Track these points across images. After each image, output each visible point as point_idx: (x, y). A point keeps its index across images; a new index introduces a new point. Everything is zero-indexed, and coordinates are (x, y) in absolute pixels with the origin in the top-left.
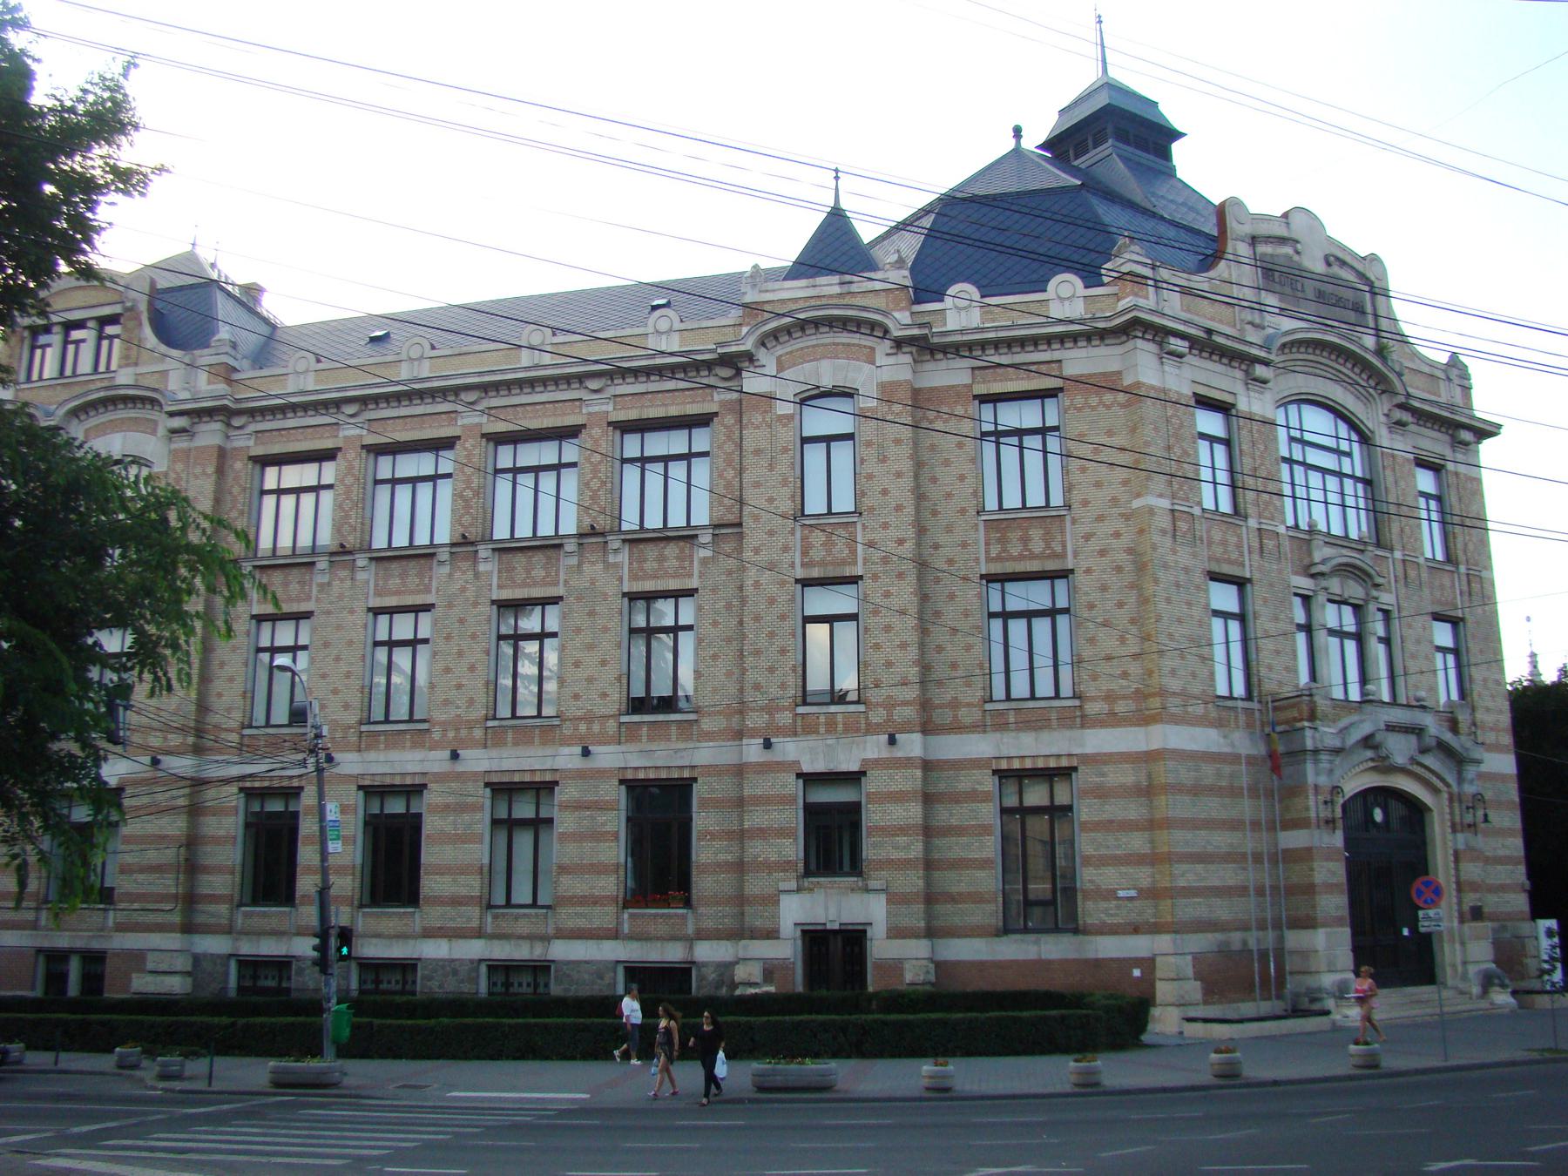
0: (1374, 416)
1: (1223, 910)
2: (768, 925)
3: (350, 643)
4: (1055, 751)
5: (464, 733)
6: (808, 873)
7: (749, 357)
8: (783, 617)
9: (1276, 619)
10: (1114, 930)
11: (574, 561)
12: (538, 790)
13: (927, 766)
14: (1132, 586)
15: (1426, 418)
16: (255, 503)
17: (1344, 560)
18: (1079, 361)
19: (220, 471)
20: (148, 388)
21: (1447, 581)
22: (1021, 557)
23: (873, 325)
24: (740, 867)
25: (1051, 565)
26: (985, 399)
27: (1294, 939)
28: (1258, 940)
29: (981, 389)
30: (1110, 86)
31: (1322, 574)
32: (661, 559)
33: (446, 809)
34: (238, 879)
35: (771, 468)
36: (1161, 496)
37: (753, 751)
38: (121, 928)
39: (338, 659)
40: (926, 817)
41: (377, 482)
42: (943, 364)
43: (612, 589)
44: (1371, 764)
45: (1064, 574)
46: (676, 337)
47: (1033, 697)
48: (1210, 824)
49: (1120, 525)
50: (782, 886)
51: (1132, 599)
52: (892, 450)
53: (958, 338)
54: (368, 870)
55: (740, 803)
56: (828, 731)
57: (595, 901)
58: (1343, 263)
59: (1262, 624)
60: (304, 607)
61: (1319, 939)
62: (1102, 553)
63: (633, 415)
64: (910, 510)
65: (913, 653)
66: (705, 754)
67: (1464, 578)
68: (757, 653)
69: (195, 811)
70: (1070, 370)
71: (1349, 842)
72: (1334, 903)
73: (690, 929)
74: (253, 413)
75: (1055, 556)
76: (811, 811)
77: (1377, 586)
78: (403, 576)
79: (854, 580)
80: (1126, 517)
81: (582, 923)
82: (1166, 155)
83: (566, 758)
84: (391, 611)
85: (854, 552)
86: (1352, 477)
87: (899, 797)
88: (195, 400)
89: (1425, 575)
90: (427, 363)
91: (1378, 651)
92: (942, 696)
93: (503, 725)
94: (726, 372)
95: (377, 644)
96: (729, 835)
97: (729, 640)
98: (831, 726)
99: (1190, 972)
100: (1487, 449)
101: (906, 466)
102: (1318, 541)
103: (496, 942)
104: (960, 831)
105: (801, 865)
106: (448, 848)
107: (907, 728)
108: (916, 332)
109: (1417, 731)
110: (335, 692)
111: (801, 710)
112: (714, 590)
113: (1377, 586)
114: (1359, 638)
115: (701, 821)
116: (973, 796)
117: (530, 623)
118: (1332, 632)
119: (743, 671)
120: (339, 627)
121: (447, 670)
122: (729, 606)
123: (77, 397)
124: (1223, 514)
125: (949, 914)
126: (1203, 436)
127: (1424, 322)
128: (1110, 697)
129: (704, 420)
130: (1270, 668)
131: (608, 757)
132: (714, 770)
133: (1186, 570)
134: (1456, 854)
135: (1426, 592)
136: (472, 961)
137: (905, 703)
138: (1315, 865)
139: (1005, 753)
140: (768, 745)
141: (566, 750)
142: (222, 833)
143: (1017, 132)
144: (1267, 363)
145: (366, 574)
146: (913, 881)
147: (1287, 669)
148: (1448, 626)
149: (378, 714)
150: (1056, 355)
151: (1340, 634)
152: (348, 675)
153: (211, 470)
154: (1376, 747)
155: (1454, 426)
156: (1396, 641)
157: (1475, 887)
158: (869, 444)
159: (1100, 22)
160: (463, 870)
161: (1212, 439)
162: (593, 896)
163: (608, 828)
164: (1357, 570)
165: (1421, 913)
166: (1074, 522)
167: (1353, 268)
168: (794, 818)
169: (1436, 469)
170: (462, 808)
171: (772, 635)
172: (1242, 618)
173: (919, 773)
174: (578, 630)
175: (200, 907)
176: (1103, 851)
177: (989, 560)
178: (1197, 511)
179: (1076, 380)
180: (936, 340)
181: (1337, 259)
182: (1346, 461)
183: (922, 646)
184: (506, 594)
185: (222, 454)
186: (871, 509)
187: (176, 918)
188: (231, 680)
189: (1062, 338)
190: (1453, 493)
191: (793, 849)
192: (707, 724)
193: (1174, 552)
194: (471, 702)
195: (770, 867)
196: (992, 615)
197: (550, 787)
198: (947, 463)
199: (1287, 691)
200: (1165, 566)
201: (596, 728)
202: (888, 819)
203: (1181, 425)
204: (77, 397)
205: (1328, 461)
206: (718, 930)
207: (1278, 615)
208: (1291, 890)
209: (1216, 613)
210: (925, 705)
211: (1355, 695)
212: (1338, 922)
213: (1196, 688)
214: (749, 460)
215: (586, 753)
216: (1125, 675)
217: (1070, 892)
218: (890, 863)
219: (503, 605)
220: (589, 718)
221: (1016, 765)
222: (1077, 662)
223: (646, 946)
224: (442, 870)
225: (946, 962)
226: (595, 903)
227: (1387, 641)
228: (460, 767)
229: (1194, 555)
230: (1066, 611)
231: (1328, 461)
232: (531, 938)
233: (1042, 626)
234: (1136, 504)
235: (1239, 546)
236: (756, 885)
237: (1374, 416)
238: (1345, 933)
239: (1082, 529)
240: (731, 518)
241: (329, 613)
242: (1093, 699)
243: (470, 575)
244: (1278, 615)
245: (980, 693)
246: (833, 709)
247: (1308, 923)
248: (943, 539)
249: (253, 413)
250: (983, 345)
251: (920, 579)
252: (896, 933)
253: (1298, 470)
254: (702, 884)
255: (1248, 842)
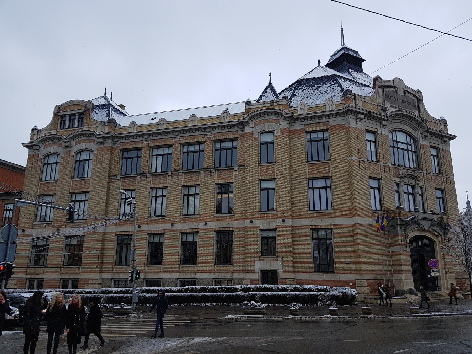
0: (418, 135)
1: (375, 268)
2: (252, 269)
3: (146, 197)
4: (327, 224)
5: (175, 219)
6: (262, 255)
7: (247, 123)
8: (255, 189)
9: (389, 189)
10: (344, 273)
11: (203, 175)
12: (186, 234)
13: (293, 227)
14: (347, 180)
15: (434, 134)
16: (121, 161)
17: (408, 173)
18: (333, 121)
19: (111, 153)
20: (91, 131)
21: (440, 179)
22: (317, 173)
23: (279, 114)
24: (245, 254)
25: (325, 175)
26: (308, 132)
27: (395, 277)
28: (385, 277)
29: (307, 130)
30: (344, 48)
31: (402, 177)
32: (225, 175)
33: (170, 239)
34: (115, 258)
35: (252, 151)
36: (356, 156)
37: (248, 223)
38: (83, 272)
39: (142, 201)
40: (293, 241)
41: (153, 156)
42: (297, 124)
43: (212, 183)
44: (417, 229)
45: (329, 177)
46: (228, 118)
47: (321, 210)
48: (370, 244)
49: (344, 164)
50: (256, 259)
51: (348, 184)
52: (284, 146)
53: (301, 116)
54: (149, 256)
55: (245, 237)
56: (267, 218)
57: (208, 263)
58: (409, 93)
59: (385, 190)
60: (133, 188)
61: (403, 276)
62: (339, 172)
63: (218, 138)
64: (288, 161)
65: (289, 198)
66: (236, 224)
67: (445, 178)
68: (249, 198)
69: (104, 241)
70: (331, 124)
71: (411, 250)
72: (407, 267)
73: (232, 270)
74: (120, 138)
75: (326, 173)
76: (262, 238)
77: (418, 180)
78: (129, 182)
79: (274, 179)
80: (346, 162)
81: (204, 268)
82: (360, 66)
83: (201, 225)
84: (156, 189)
85: (273, 172)
86: (411, 151)
87: (285, 235)
88: (104, 134)
89: (433, 177)
90: (165, 125)
91: (418, 198)
92: (296, 209)
93: (186, 216)
94: (241, 127)
95: (152, 197)
96: (242, 245)
97: (242, 195)
98: (268, 218)
99: (366, 285)
100: (452, 142)
101: (287, 150)
102: (401, 168)
103: (182, 274)
104: (302, 245)
105: (260, 253)
106: (170, 249)
107: (287, 217)
108: (290, 115)
109: (431, 220)
110: (142, 209)
111: (260, 213)
112: (238, 182)
113: (418, 180)
114: (413, 194)
115: (235, 241)
116: (305, 235)
117: (192, 191)
118: (405, 193)
119: (245, 203)
120: (143, 193)
121: (171, 203)
122: (242, 186)
123: (72, 134)
124: (373, 161)
125: (299, 267)
126: (368, 140)
127: (433, 108)
128: (342, 210)
129: (236, 139)
130: (387, 202)
131: (211, 225)
132: (238, 228)
133: (363, 176)
134: (444, 254)
135: (433, 182)
136: (175, 279)
137: (287, 211)
138: (402, 256)
139: (314, 224)
140: (252, 222)
141: (201, 223)
142: (111, 246)
143: (319, 61)
144: (386, 120)
145: (150, 179)
146: (290, 258)
147: (392, 203)
148: (440, 191)
149: (153, 215)
150: (327, 120)
151: (408, 193)
152: (145, 205)
153: (109, 152)
154: (419, 224)
155: (440, 136)
156: (424, 196)
157: (450, 264)
158: (278, 145)
159: (343, 30)
160: (174, 255)
161: (370, 141)
162: (207, 261)
163: (211, 243)
164: (412, 177)
165: (432, 270)
166: (332, 164)
167: (413, 95)
168: (258, 240)
169: (437, 148)
170: (174, 239)
171: (253, 194)
172: (379, 189)
173: (291, 229)
174: (204, 193)
175: (104, 266)
176: (341, 251)
177: (309, 174)
178: (366, 160)
179: (334, 126)
180: (295, 117)
181: (407, 91)
182: (409, 147)
183: (291, 196)
184: (186, 184)
185: (112, 148)
186: (278, 161)
187: (98, 269)
188: (114, 206)
189: (329, 116)
190: (442, 154)
191: (258, 249)
192: (236, 216)
193: (360, 171)
194: (177, 211)
195: (252, 253)
196: (309, 188)
197: (197, 233)
198: (298, 149)
199: (393, 208)
200: (357, 175)
201: (208, 218)
202: (283, 242)
203: (362, 138)
204: (72, 134)
205: (404, 147)
206: (239, 270)
207: (389, 190)
208: (394, 263)
209: (371, 188)
210: (292, 211)
211: (412, 210)
212: (409, 272)
213: (366, 207)
214: (247, 149)
215: (206, 224)
216: (346, 204)
217: (332, 262)
218: (283, 253)
219: (185, 187)
220: (207, 215)
221: (317, 227)
222: (332, 199)
223: (220, 274)
224: (168, 255)
225: (298, 280)
226: (208, 263)
227: (422, 195)
228: (174, 228)
229: (365, 172)
230: (330, 187)
231: (404, 147)
232: (191, 273)
233: (323, 191)
234: (349, 159)
235: (378, 170)
236: (249, 258)
237: (418, 135)
238: (411, 275)
239: (334, 165)
240: (242, 164)
241: (140, 189)
242: (337, 210)
243: (177, 179)
244: (389, 190)
245: (307, 208)
246: (268, 212)
247: (400, 272)
248: (297, 169)
249: (120, 138)
250: (308, 118)
251: (291, 179)
252: (285, 272)
253: (395, 149)
254: (235, 258)
255: (384, 249)
